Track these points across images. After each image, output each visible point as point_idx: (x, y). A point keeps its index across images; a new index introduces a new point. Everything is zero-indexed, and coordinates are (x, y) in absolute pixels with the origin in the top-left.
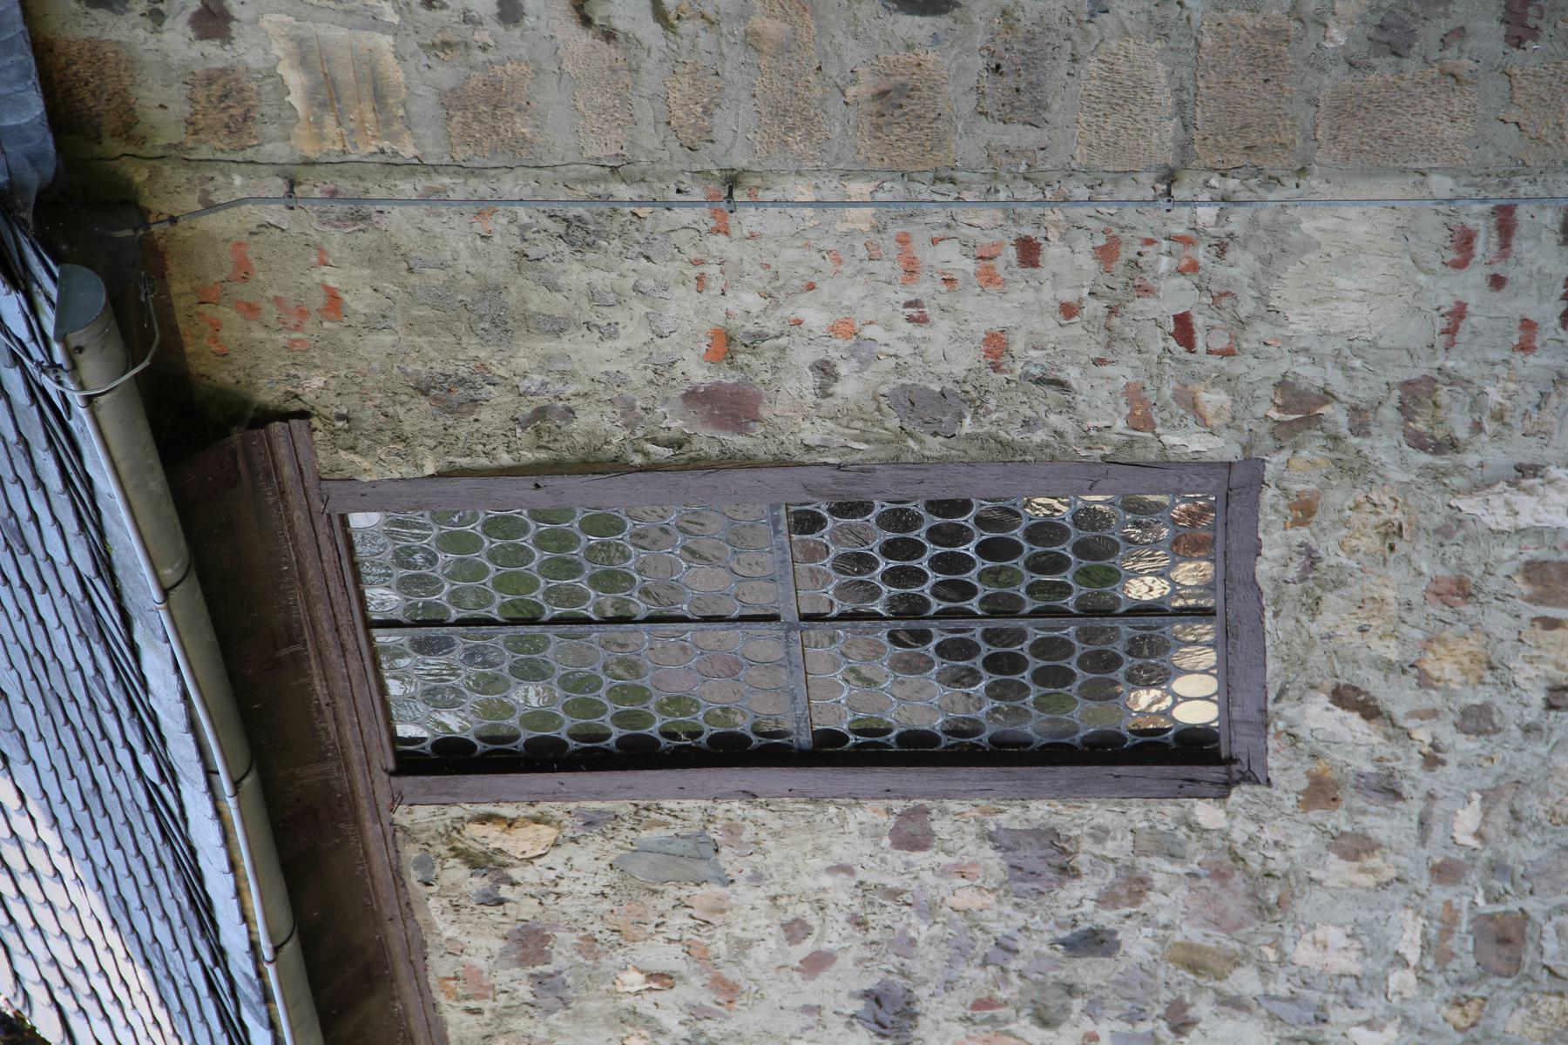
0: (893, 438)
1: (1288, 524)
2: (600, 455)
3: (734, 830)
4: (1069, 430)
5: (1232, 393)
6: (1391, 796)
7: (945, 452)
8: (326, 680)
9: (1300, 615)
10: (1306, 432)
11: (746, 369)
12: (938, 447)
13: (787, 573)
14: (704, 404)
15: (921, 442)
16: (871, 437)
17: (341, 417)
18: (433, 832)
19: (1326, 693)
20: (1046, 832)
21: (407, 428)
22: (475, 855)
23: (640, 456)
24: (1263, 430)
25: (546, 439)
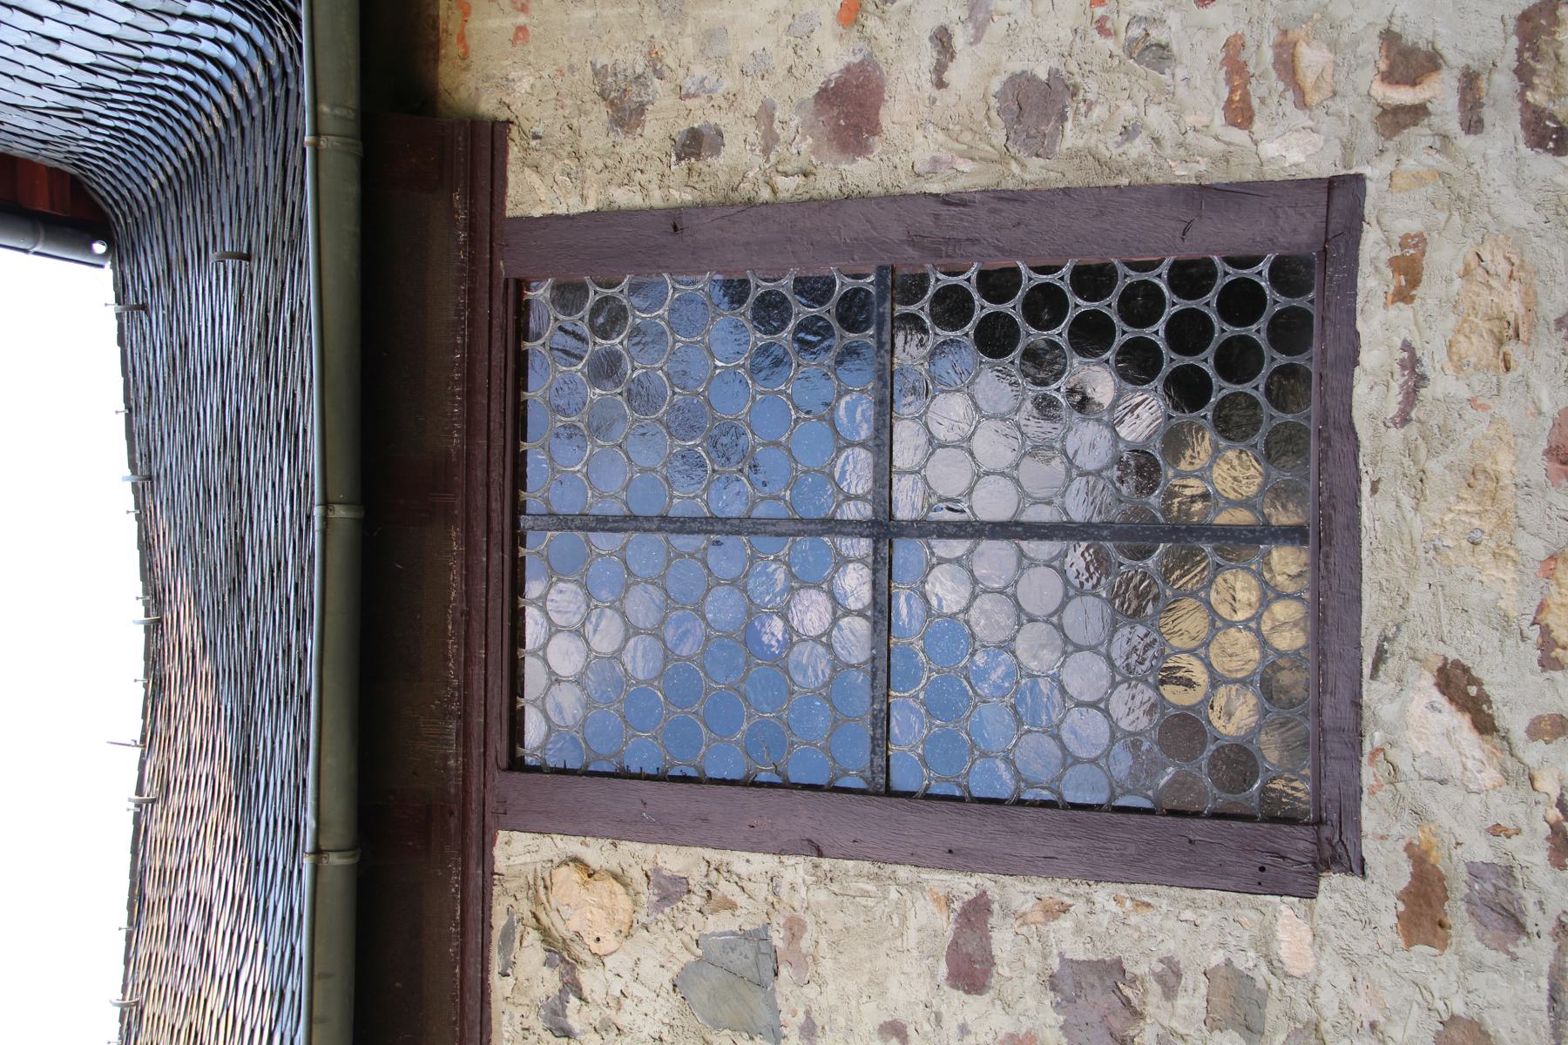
0: (997, 157)
1: (1390, 297)
2: (735, 197)
3: (805, 905)
4: (1167, 134)
5: (1333, 46)
6: (1512, 926)
7: (1044, 175)
8: (467, 570)
9: (1401, 495)
10: (1412, 129)
11: (873, 41)
12: (1038, 170)
13: (884, 426)
14: (832, 105)
15: (1023, 166)
16: (976, 155)
17: (536, 137)
18: (522, 881)
19: (1431, 672)
20: (1111, 966)
21: (584, 145)
22: (555, 939)
23: (769, 190)
24: (1366, 116)
25: (695, 179)
